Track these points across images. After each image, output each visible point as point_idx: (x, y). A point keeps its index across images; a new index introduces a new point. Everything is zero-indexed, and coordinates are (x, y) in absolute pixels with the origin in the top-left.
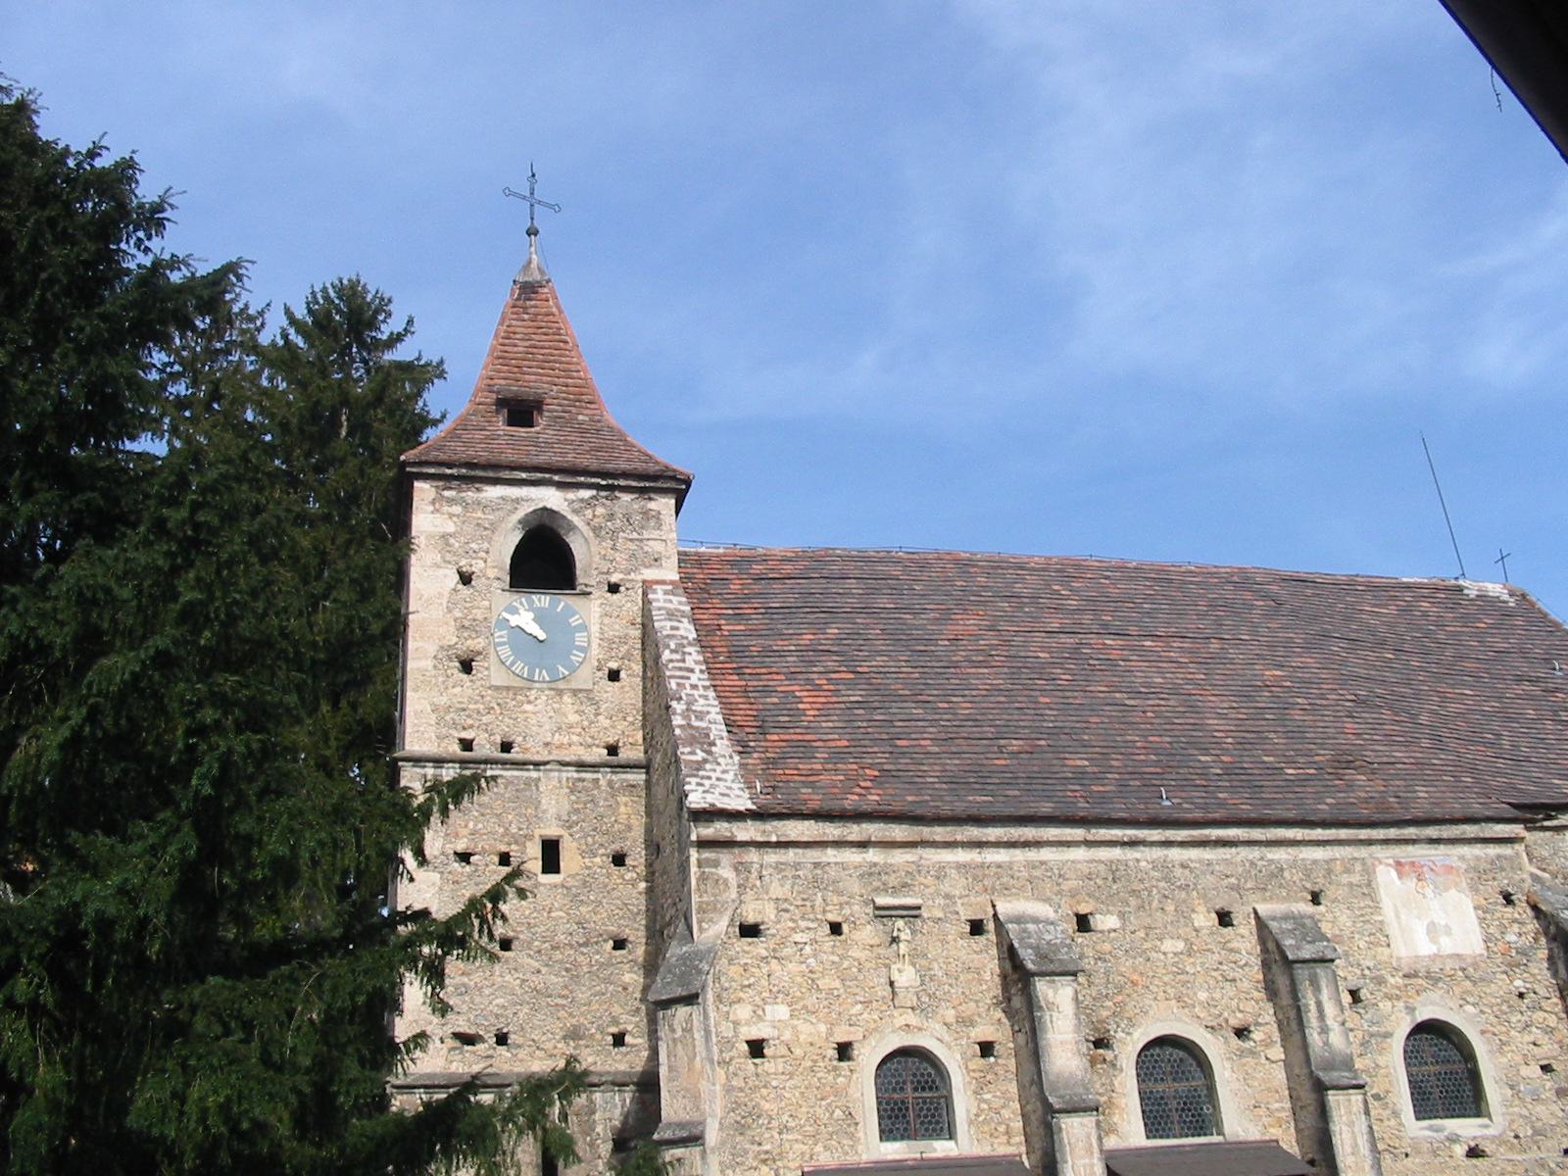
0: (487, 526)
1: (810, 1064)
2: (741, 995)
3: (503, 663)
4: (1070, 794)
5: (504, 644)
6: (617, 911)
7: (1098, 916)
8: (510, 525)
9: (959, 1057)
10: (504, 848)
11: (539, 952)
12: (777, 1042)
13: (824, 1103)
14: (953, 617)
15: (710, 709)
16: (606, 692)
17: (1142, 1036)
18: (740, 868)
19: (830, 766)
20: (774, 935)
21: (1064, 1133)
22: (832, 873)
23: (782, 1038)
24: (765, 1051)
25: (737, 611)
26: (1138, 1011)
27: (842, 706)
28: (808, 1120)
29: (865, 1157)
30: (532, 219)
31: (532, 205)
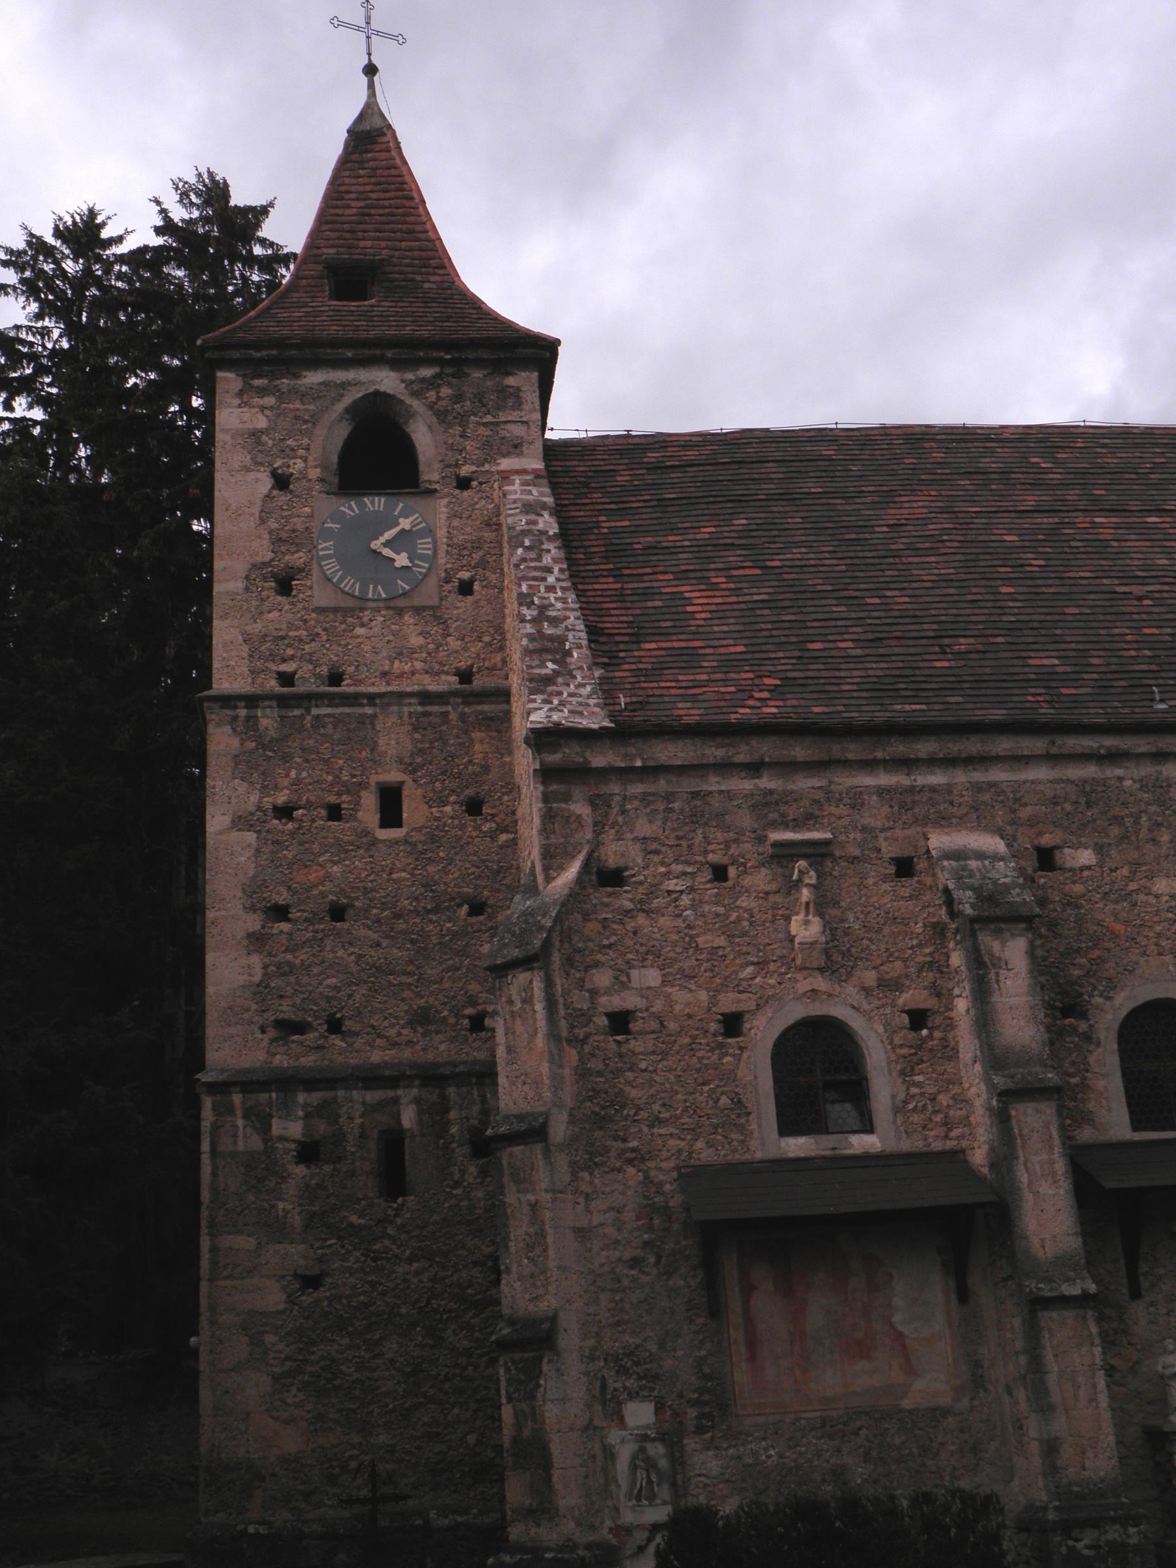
0: (306, 418)
1: (687, 1040)
2: (599, 957)
3: (329, 580)
4: (1030, 698)
5: (328, 557)
6: (473, 869)
7: (1067, 851)
8: (335, 416)
9: (881, 1030)
10: (332, 799)
11: (378, 921)
12: (645, 1014)
13: (706, 1088)
14: (896, 499)
15: (568, 613)
16: (457, 608)
17: (1124, 1001)
18: (598, 802)
19: (718, 676)
20: (641, 883)
21: (1014, 1122)
22: (716, 803)
23: (652, 1010)
24: (631, 1026)
25: (622, 506)
26: (1121, 970)
27: (743, 606)
28: (685, 1110)
29: (759, 1155)
30: (369, 54)
31: (368, 37)
